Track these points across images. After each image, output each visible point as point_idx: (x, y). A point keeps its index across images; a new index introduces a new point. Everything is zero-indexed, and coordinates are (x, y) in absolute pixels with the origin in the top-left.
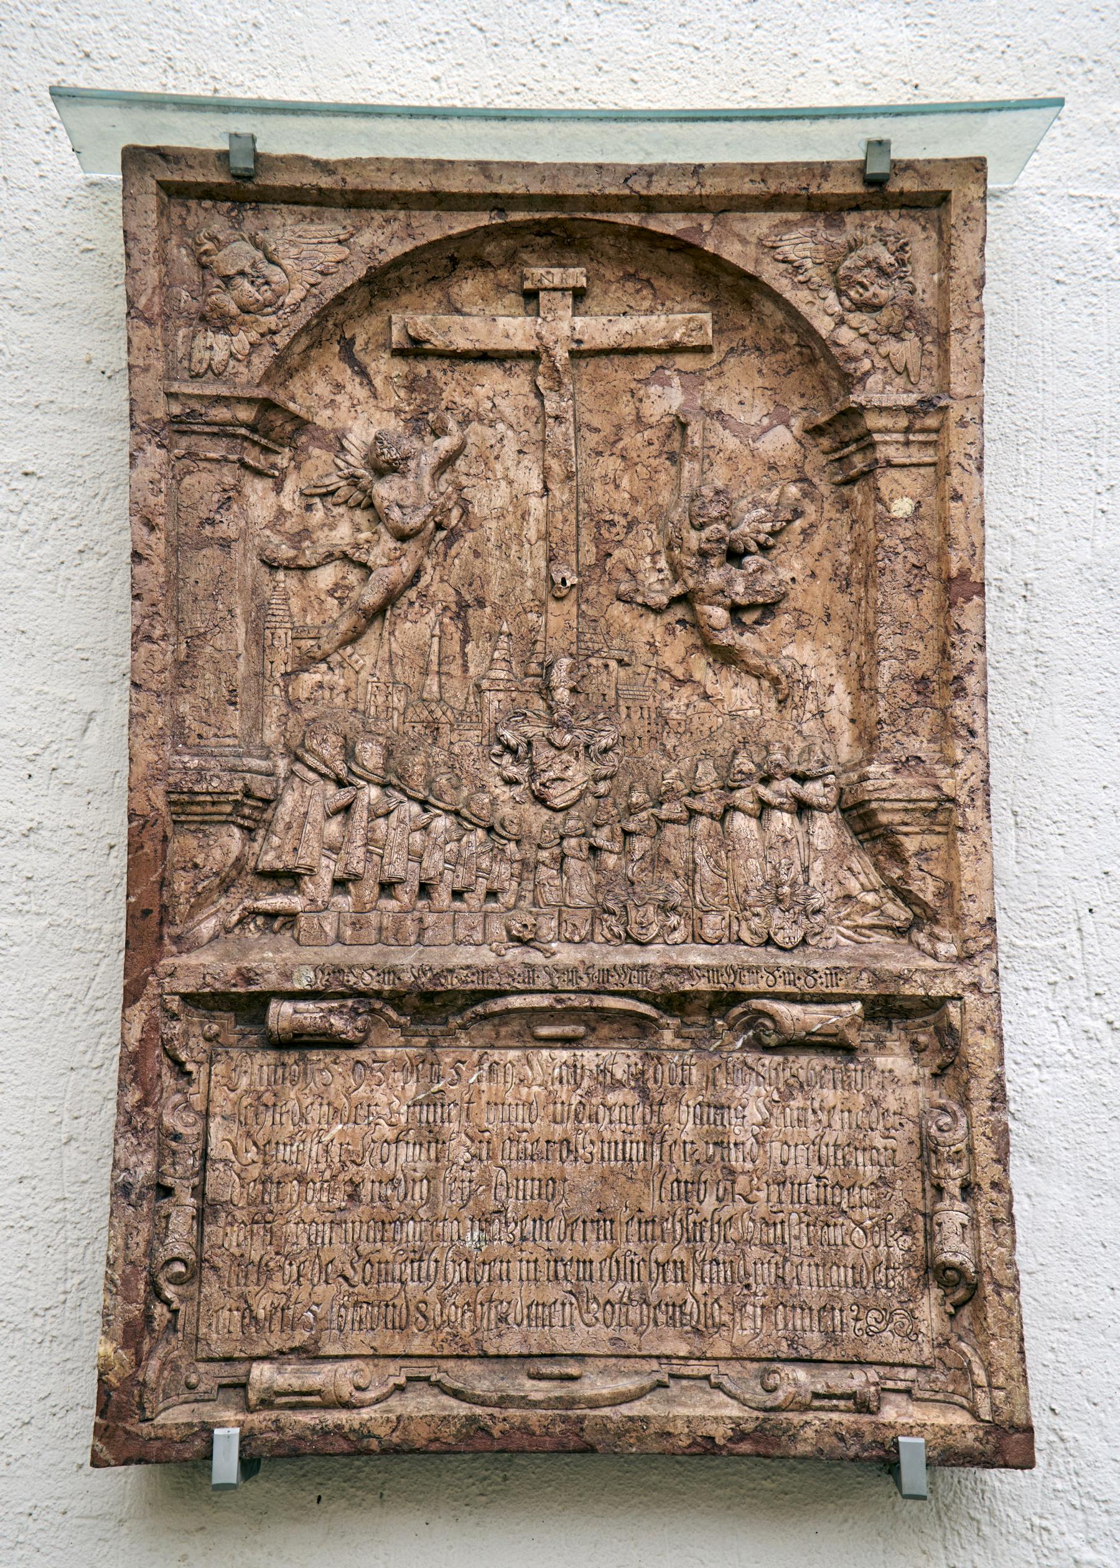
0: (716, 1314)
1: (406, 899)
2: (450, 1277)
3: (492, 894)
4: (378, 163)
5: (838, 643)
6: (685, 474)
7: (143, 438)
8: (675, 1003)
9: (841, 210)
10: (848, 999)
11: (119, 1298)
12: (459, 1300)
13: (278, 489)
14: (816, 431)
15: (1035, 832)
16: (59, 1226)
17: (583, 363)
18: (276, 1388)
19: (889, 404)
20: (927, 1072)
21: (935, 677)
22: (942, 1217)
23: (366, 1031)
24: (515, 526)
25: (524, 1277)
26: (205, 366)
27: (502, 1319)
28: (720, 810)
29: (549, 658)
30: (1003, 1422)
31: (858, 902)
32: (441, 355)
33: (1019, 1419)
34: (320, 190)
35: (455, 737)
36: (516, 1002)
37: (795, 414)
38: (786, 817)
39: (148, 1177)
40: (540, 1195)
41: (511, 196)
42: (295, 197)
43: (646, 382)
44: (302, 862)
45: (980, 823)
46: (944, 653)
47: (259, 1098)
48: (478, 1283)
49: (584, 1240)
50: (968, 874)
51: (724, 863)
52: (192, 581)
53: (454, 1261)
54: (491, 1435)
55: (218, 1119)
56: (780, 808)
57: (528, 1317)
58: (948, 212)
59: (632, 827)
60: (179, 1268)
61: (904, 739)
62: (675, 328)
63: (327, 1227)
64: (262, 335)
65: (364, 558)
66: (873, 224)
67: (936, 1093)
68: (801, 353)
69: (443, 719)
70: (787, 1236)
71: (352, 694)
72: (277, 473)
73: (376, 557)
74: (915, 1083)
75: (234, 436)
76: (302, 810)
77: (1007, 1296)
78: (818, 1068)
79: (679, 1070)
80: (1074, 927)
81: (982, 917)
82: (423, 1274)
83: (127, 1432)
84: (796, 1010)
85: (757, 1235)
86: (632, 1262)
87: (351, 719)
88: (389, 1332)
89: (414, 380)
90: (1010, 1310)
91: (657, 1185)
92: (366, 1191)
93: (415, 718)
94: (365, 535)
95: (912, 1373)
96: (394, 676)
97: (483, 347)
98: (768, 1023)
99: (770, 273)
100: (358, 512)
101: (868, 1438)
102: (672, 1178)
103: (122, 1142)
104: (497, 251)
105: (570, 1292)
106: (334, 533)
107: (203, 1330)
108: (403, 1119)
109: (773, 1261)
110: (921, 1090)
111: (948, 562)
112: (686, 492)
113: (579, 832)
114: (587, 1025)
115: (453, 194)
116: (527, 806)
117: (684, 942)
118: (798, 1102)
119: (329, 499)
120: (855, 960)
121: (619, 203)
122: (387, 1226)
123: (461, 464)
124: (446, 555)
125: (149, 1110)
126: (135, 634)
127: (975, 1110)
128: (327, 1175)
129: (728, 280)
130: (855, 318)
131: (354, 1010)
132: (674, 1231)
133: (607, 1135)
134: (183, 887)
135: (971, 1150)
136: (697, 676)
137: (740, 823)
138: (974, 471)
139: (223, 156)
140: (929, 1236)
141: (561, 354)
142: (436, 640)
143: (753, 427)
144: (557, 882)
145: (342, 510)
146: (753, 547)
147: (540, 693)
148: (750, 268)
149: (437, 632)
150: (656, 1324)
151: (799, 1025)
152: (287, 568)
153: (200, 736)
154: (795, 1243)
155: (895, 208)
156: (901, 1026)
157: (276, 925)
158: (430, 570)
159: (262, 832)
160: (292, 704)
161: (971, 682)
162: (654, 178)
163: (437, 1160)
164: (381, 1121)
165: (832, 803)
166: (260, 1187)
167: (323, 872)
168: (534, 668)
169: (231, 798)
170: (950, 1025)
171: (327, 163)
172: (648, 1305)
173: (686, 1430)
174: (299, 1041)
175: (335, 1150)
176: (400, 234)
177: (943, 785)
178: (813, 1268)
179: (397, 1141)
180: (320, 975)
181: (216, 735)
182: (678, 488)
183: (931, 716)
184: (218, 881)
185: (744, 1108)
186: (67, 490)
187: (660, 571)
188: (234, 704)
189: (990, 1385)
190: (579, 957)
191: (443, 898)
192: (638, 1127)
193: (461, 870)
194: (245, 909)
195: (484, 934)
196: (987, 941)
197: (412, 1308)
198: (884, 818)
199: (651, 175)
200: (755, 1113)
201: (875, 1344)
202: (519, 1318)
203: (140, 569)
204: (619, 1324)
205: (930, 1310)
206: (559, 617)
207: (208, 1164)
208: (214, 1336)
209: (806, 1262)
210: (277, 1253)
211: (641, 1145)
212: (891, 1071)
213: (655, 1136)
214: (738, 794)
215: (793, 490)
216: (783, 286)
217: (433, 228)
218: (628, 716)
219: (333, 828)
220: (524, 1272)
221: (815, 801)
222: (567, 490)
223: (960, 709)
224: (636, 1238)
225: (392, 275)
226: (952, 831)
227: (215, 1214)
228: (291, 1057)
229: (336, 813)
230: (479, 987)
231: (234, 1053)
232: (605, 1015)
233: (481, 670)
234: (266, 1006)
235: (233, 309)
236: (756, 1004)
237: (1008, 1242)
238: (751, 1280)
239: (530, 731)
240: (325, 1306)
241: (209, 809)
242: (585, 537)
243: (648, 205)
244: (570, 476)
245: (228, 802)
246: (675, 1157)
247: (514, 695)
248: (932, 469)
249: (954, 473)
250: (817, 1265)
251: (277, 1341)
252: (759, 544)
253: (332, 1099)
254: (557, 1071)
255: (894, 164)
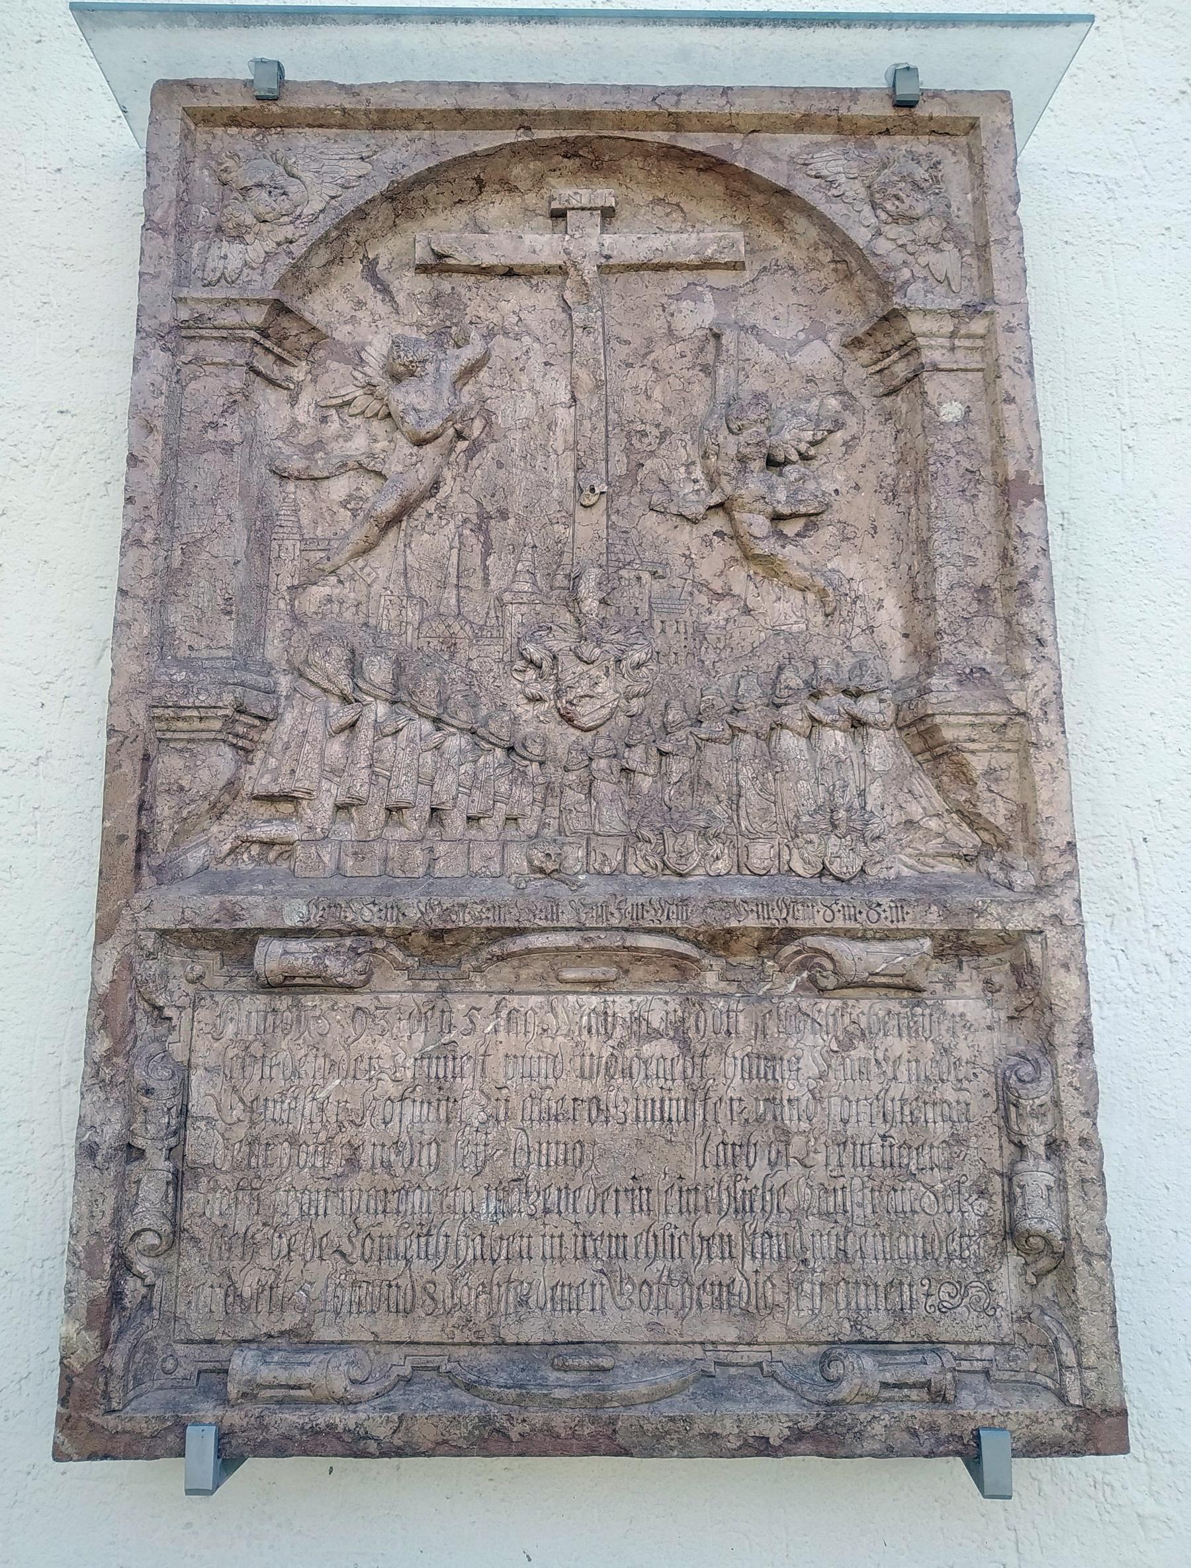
0: (769, 1293)
1: (415, 826)
2: (462, 1254)
3: (512, 819)
4: (404, 85)
5: (886, 555)
6: (721, 382)
7: (149, 342)
8: (719, 942)
9: (871, 134)
10: (915, 935)
11: (83, 1273)
12: (474, 1280)
13: (294, 401)
14: (857, 343)
15: (1086, 759)
16: (58, 1173)
17: (612, 279)
18: (259, 1380)
19: (934, 307)
20: (1003, 1015)
21: (997, 585)
22: (1026, 1179)
23: (368, 974)
24: (540, 436)
25: (548, 1255)
26: (218, 274)
27: (523, 1302)
28: (766, 728)
29: (576, 570)
30: (1095, 1406)
31: (920, 827)
32: (467, 271)
33: (1112, 1403)
34: (344, 110)
35: (473, 653)
36: (537, 941)
37: (832, 330)
38: (839, 735)
39: (119, 1137)
40: (565, 1160)
41: (537, 113)
42: (319, 120)
43: (678, 298)
44: (299, 785)
45: (1054, 739)
46: (1005, 558)
47: (247, 1048)
48: (494, 1261)
49: (617, 1212)
50: (1044, 795)
51: (771, 786)
52: (191, 486)
53: (466, 1236)
54: (509, 1437)
55: (201, 1072)
56: (832, 725)
57: (552, 1299)
58: (978, 137)
59: (667, 747)
60: (150, 1239)
61: (966, 650)
62: (707, 246)
63: (321, 1197)
64: (279, 244)
65: (378, 467)
66: (903, 148)
67: (1013, 1040)
68: (835, 270)
69: (461, 634)
70: (848, 1204)
71: (363, 608)
72: (292, 386)
73: (393, 468)
74: (989, 1028)
75: (243, 339)
76: (301, 728)
77: (1098, 1264)
78: (881, 1014)
79: (724, 1017)
80: (1129, 857)
81: (1061, 842)
82: (431, 1250)
83: (92, 1425)
84: (858, 948)
85: (815, 1203)
86: (672, 1236)
87: (361, 633)
88: (393, 1316)
89: (438, 296)
90: (1102, 1281)
91: (700, 1148)
92: (365, 1157)
93: (431, 633)
94: (379, 446)
95: (989, 1351)
96: (409, 590)
97: (509, 262)
98: (828, 965)
99: (803, 187)
100: (375, 423)
101: (944, 1432)
102: (716, 1140)
103: (88, 1097)
104: (524, 174)
105: (601, 1271)
106: (349, 444)
107: (182, 1308)
108: (409, 1074)
109: (834, 1232)
110: (996, 1035)
111: (1005, 465)
112: (721, 398)
113: (609, 753)
114: (618, 965)
115: (478, 111)
116: (552, 725)
117: (728, 874)
118: (861, 1050)
119: (346, 409)
120: (921, 891)
121: (650, 119)
122: (390, 1196)
123: (484, 375)
124: (467, 466)
125: (119, 1060)
126: (125, 538)
127: (1060, 1060)
128: (323, 1137)
129: (759, 199)
130: (892, 231)
131: (353, 949)
132: (720, 1201)
133: (643, 1092)
134: (167, 812)
135: (1057, 1103)
136: (736, 590)
137: (789, 742)
138: (1026, 374)
139: (247, 84)
140: (1010, 1199)
141: (589, 269)
142: (455, 551)
143: (791, 340)
144: (585, 808)
145: (358, 421)
146: (794, 457)
147: (567, 606)
148: (782, 183)
149: (456, 544)
150: (700, 1305)
151: (861, 966)
152: (298, 479)
153: (191, 648)
154: (858, 1211)
155: (924, 134)
156: (973, 964)
157: (272, 855)
158: (449, 481)
159: (260, 755)
160: (297, 619)
161: (1037, 587)
162: (683, 97)
163: (448, 1121)
164: (384, 1076)
165: (890, 720)
166: (245, 1149)
167: (323, 796)
168: (560, 581)
169: (220, 712)
170: (1030, 964)
171: (352, 86)
172: (691, 1285)
173: (736, 1431)
174: (284, 985)
175: (331, 1109)
176: (424, 151)
177: (1013, 698)
178: (879, 1238)
179: (402, 1099)
180: (314, 911)
181: (208, 647)
182: (713, 397)
183: (996, 627)
184: (206, 806)
185: (798, 1059)
186: (98, 426)
187: (695, 481)
188: (229, 613)
189: (1079, 1364)
190: (610, 890)
191: (456, 823)
192: (679, 1082)
193: (477, 794)
194: (237, 837)
195: (503, 865)
196: (1068, 868)
197: (418, 1289)
198: (948, 734)
199: (679, 95)
200: (810, 1066)
201: (948, 1321)
202: (541, 1303)
203: (137, 474)
204: (658, 1309)
205: (1008, 1278)
206: (590, 525)
207: (189, 1122)
208: (194, 1315)
209: (870, 1232)
210: (265, 1224)
211: (682, 1103)
212: (962, 1015)
213: (698, 1093)
214: (785, 711)
215: (833, 403)
216: (817, 199)
217: (458, 144)
218: (663, 631)
219: (335, 748)
220: (548, 1249)
221: (871, 719)
222: (596, 399)
223: (1027, 617)
224: (676, 1209)
225: (417, 193)
226: (1027, 748)
227: (197, 1177)
228: (283, 1002)
229: (342, 730)
230: (494, 925)
231: (219, 998)
232: (639, 956)
233: (504, 584)
234: (253, 944)
235: (249, 219)
236: (811, 941)
237: (1099, 1204)
238: (809, 1255)
239: (556, 646)
240: (319, 1285)
241: (197, 725)
242: (616, 445)
243: (676, 122)
244: (599, 385)
245: (216, 717)
246: (720, 1117)
247: (538, 608)
248: (980, 374)
249: (1005, 376)
250: (883, 1235)
251: (263, 1322)
252: (800, 454)
253: (329, 1050)
254: (585, 1018)
255: (923, 92)
